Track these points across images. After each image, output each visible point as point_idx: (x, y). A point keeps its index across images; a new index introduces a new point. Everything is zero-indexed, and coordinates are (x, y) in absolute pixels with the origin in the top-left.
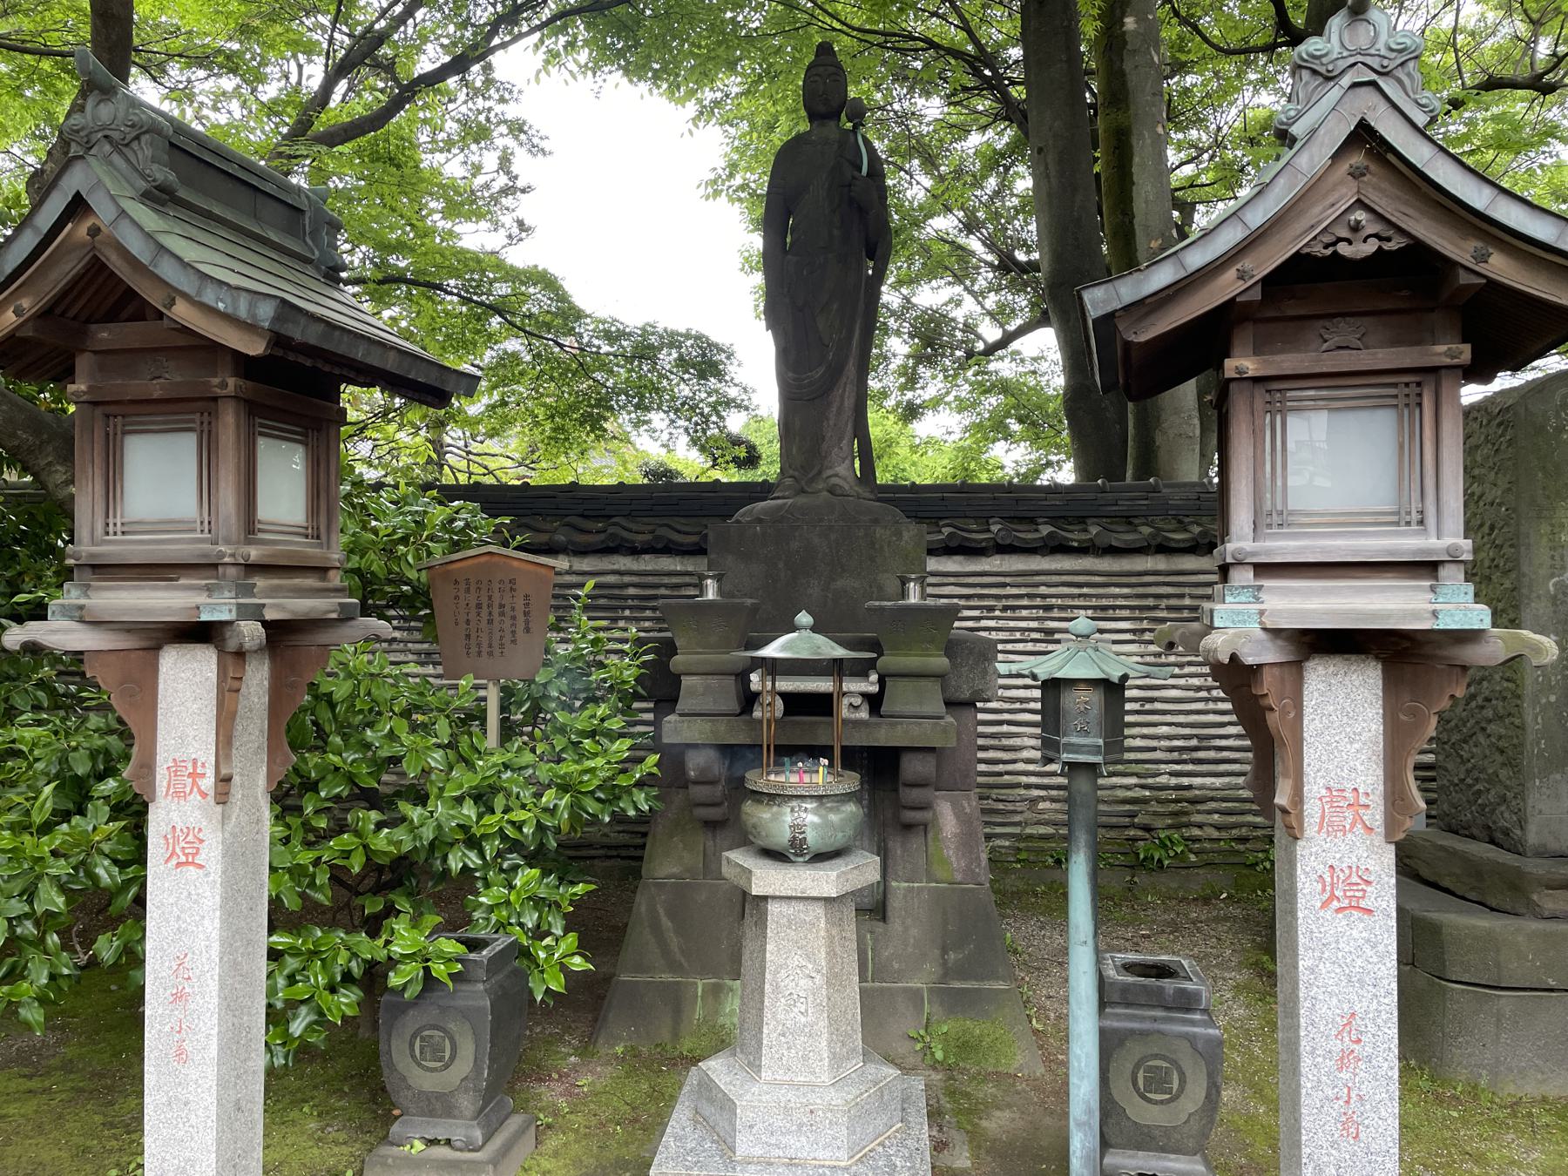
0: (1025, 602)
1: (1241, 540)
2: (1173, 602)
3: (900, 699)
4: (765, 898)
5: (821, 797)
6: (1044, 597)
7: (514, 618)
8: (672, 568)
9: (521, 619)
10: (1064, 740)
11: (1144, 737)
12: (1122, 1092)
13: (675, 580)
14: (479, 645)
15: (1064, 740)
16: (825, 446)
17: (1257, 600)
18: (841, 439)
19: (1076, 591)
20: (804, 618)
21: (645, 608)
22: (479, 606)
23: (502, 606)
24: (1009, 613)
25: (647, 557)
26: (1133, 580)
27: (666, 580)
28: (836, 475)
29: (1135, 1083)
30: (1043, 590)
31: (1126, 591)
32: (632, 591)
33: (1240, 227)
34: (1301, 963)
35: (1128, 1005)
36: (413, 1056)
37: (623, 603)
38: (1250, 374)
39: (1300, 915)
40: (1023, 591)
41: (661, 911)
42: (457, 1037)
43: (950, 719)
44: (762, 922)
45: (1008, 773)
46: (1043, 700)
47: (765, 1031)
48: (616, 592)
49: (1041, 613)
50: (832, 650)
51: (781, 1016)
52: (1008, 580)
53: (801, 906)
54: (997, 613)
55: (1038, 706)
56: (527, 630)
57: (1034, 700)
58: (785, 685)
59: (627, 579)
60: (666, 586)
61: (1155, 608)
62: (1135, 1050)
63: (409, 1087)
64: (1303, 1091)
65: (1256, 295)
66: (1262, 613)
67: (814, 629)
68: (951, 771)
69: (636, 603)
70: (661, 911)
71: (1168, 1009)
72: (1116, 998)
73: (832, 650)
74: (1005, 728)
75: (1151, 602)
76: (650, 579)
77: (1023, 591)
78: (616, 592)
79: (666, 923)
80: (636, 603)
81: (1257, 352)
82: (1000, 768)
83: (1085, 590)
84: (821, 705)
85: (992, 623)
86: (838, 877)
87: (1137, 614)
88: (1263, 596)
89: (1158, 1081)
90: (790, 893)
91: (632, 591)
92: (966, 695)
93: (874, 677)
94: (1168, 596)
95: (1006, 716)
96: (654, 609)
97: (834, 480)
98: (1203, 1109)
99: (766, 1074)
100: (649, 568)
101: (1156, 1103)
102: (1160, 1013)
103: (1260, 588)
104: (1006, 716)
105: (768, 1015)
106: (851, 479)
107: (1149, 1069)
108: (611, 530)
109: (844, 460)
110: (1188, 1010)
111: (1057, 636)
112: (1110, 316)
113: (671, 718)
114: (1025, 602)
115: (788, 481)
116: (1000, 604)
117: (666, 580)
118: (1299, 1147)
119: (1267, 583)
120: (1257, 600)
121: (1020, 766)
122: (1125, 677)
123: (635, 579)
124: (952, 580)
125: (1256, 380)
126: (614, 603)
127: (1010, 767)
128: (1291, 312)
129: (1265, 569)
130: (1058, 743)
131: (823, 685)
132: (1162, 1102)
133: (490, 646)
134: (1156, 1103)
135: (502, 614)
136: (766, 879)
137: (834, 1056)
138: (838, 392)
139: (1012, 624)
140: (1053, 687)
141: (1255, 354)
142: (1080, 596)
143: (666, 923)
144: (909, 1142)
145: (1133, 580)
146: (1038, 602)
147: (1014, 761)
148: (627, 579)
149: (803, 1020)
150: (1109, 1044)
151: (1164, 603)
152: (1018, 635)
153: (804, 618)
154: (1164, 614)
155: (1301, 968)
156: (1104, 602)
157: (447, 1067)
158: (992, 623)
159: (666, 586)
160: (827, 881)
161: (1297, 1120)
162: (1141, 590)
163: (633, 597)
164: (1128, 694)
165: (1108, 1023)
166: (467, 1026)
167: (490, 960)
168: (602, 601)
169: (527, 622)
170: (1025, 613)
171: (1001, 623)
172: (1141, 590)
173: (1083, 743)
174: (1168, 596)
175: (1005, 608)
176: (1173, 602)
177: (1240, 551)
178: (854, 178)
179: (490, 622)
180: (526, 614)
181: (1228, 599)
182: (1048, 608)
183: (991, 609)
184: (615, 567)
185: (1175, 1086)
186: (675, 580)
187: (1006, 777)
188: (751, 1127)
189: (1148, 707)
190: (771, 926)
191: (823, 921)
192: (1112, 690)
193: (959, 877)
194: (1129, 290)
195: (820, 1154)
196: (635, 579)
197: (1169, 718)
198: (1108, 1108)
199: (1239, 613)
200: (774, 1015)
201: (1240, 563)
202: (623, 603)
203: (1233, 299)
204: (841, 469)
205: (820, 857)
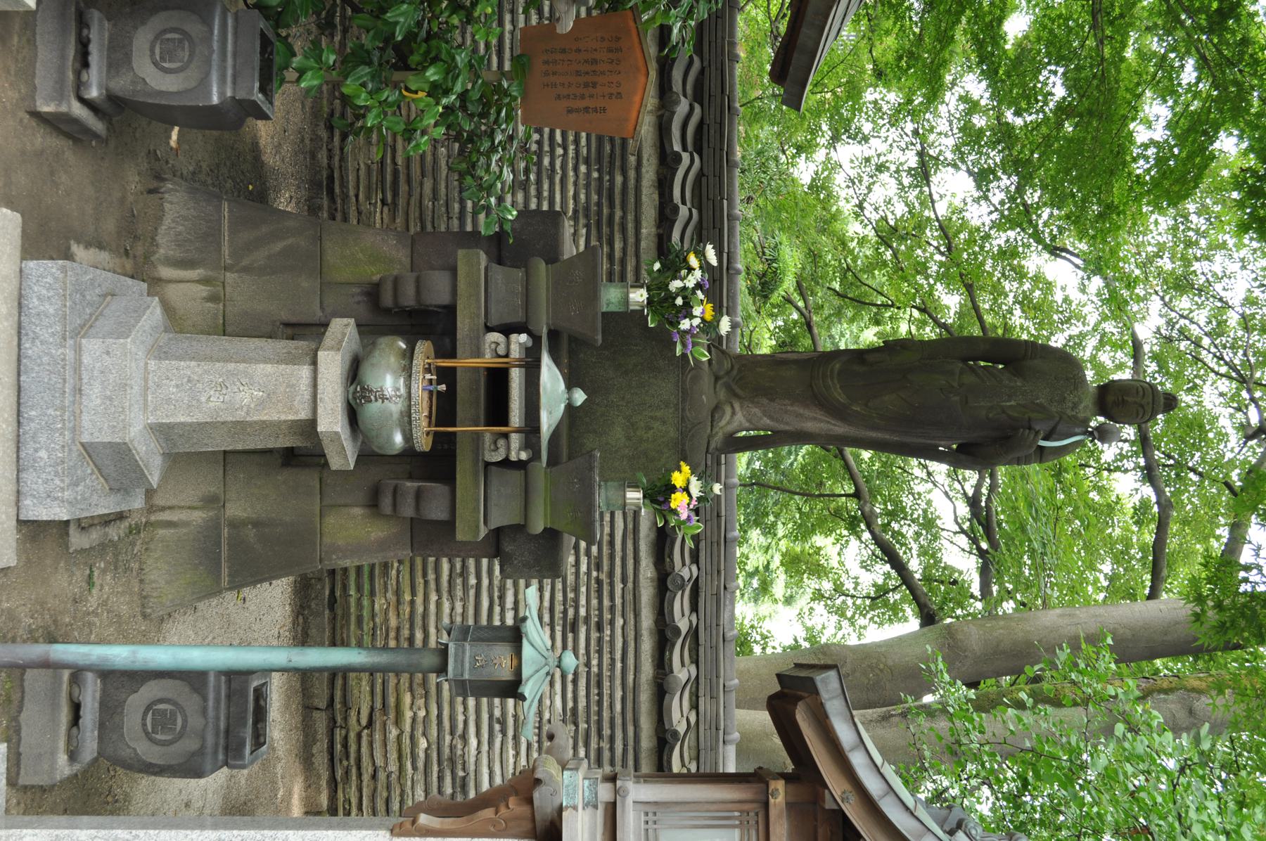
0: (606, 603)
1: (638, 792)
2: (606, 754)
3: (506, 488)
4: (314, 363)
5: (410, 416)
6: (612, 622)
7: (583, 97)
8: (644, 224)
9: (581, 104)
10: (467, 647)
11: (466, 722)
12: (150, 691)
13: (630, 226)
14: (555, 62)
15: (467, 647)
16: (765, 401)
17: (586, 806)
18: (771, 418)
19: (618, 656)
20: (580, 397)
21: (599, 194)
22: (595, 62)
23: (594, 85)
24: (594, 585)
25: (656, 196)
26: (629, 716)
27: (630, 217)
28: (734, 413)
29: (161, 701)
30: (619, 622)
31: (618, 707)
32: (619, 179)
33: (880, 793)
34: (291, 832)
35: (229, 697)
36: (165, 31)
37: (606, 169)
38: (772, 801)
39: (330, 832)
40: (618, 601)
41: (290, 241)
42: (182, 75)
43: (483, 532)
44: (292, 360)
45: (426, 583)
46: (539, 210)
47: (193, 363)
48: (618, 163)
49: (594, 619)
50: (548, 420)
51: (206, 378)
52: (630, 585)
53: (307, 396)
54: (594, 574)
55: (497, 623)
56: (570, 111)
57: (539, 204)
58: (516, 376)
59: (632, 174)
60: (624, 217)
61: (600, 736)
62: (191, 702)
63: (136, 28)
64: (189, 832)
65: (829, 805)
66: (575, 808)
67: (570, 407)
68: (432, 536)
69: (606, 184)
70: (290, 241)
71: (227, 731)
72: (234, 685)
73: (548, 420)
74: (473, 581)
75: (606, 732)
76: (632, 200)
77: (618, 601)
78: (618, 163)
79: (279, 246)
80: (606, 184)
81: (790, 805)
82: (431, 576)
83: (619, 665)
84: (497, 413)
85: (584, 568)
86: (336, 433)
87: (594, 718)
88: (589, 810)
89: (163, 722)
90: (320, 387)
91: (619, 179)
92: (508, 547)
93: (524, 456)
94: (612, 749)
95: (485, 582)
96: (599, 204)
97: (728, 410)
98: (140, 760)
99: (152, 364)
100: (644, 198)
101: (144, 719)
102: (222, 725)
103: (596, 807)
104: (485, 582)
105: (206, 366)
106: (730, 428)
107: (173, 714)
108: (686, 157)
109: (749, 421)
110: (226, 748)
111: (570, 635)
112: (816, 692)
113: (483, 257)
114: (606, 603)
115: (727, 365)
116: (603, 576)
117: (630, 217)
118: (143, 828)
119: (600, 813)
120: (586, 806)
121: (433, 597)
122: (523, 698)
123: (632, 182)
124: (630, 526)
125: (766, 805)
126: (606, 160)
127: (432, 585)
128: (820, 831)
129: (611, 812)
130: (465, 640)
131: (516, 416)
132: (144, 725)
133: (554, 73)
134: (144, 719)
135: (586, 85)
136: (332, 365)
137: (171, 426)
138: (819, 414)
139: (583, 589)
140: (515, 636)
141: (787, 804)
142: (613, 660)
143: (279, 246)
144: (95, 497)
145: (629, 716)
146: (607, 616)
147: (438, 590)
148: (632, 174)
149: (203, 399)
150: (194, 679)
151: (605, 745)
152: (571, 595)
153: (580, 397)
154: (594, 745)
155: (287, 832)
156: (606, 684)
157: (155, 64)
158: (584, 568)
159: (624, 217)
160: (331, 422)
161: (164, 828)
162: (618, 721)
163: (612, 181)
164: (511, 702)
165: (212, 679)
166: (193, 84)
167: (254, 102)
168: (608, 148)
169: (578, 110)
170: (594, 602)
171: (584, 578)
172: (618, 721)
173: (467, 660)
174: (612, 749)
175: (599, 581)
176: (606, 754)
177: (626, 793)
178: (1037, 433)
179: (578, 73)
180: (586, 109)
181: (587, 782)
182: (599, 627)
183: (599, 567)
184: (645, 161)
185: (159, 737)
186: (630, 226)
187: (422, 581)
188: (108, 353)
189: (497, 727)
190: (288, 369)
191: (291, 417)
192: (512, 689)
193: (327, 540)
194: (834, 707)
195: (85, 417)
196: (632, 182)
197: (485, 747)
198: (137, 677)
199: (575, 791)
200: (206, 372)
201: (616, 792)
202: (606, 169)
203: (826, 786)
204: (739, 417)
205: (353, 415)
